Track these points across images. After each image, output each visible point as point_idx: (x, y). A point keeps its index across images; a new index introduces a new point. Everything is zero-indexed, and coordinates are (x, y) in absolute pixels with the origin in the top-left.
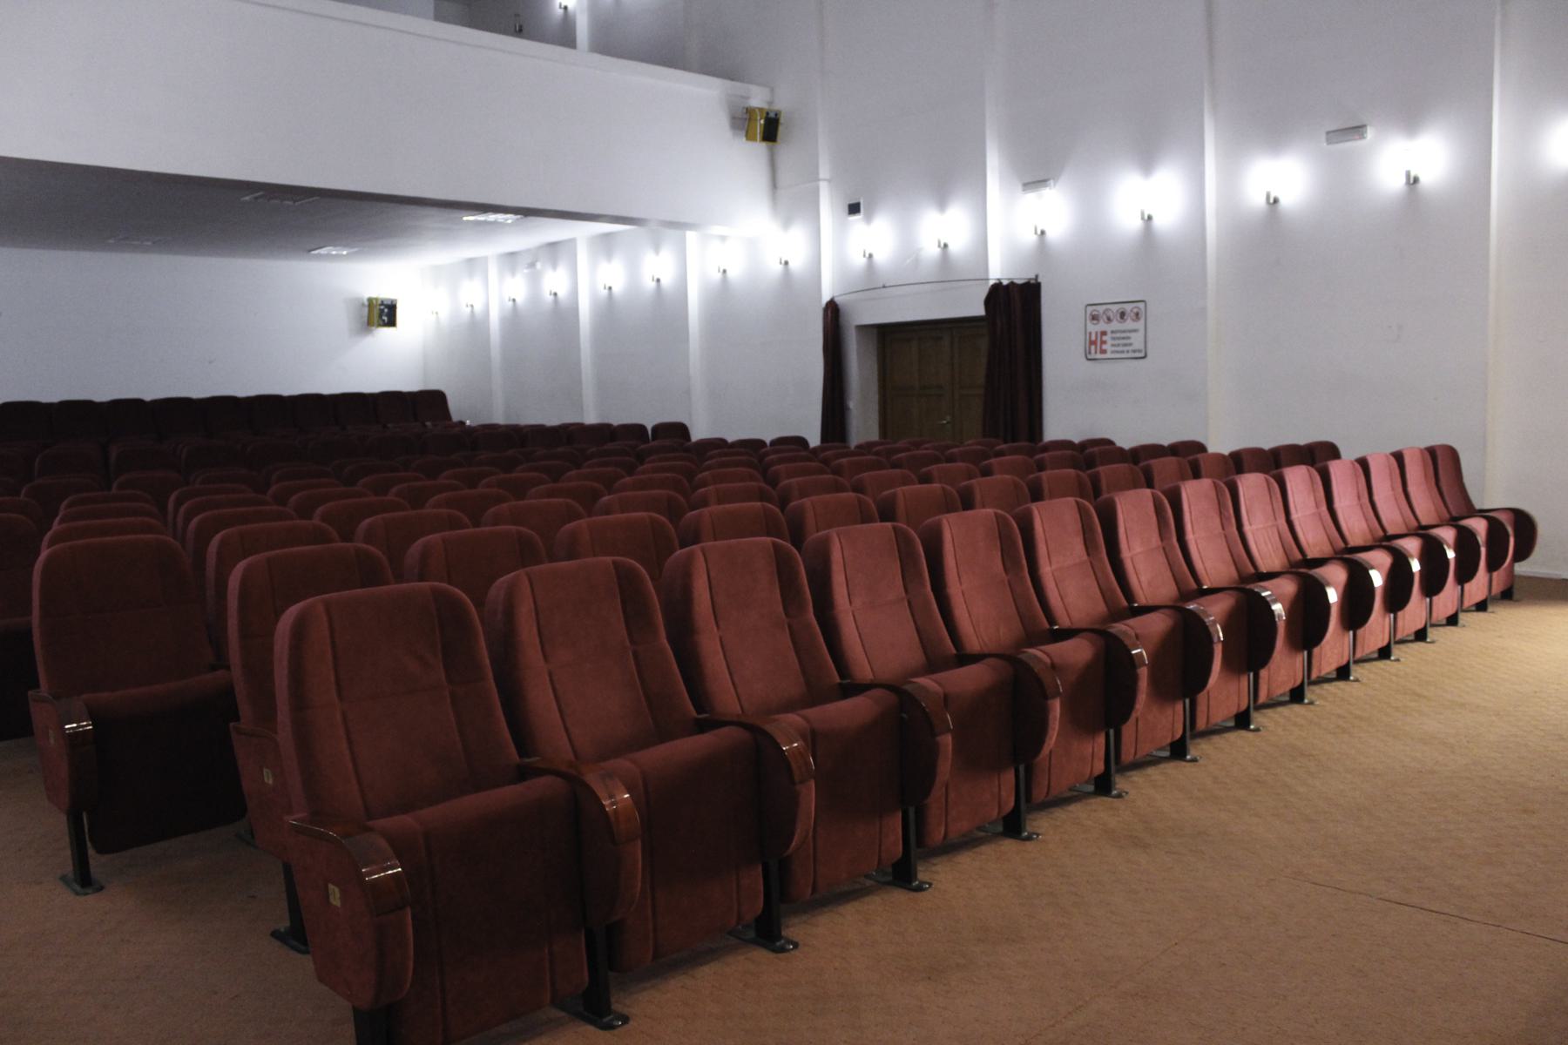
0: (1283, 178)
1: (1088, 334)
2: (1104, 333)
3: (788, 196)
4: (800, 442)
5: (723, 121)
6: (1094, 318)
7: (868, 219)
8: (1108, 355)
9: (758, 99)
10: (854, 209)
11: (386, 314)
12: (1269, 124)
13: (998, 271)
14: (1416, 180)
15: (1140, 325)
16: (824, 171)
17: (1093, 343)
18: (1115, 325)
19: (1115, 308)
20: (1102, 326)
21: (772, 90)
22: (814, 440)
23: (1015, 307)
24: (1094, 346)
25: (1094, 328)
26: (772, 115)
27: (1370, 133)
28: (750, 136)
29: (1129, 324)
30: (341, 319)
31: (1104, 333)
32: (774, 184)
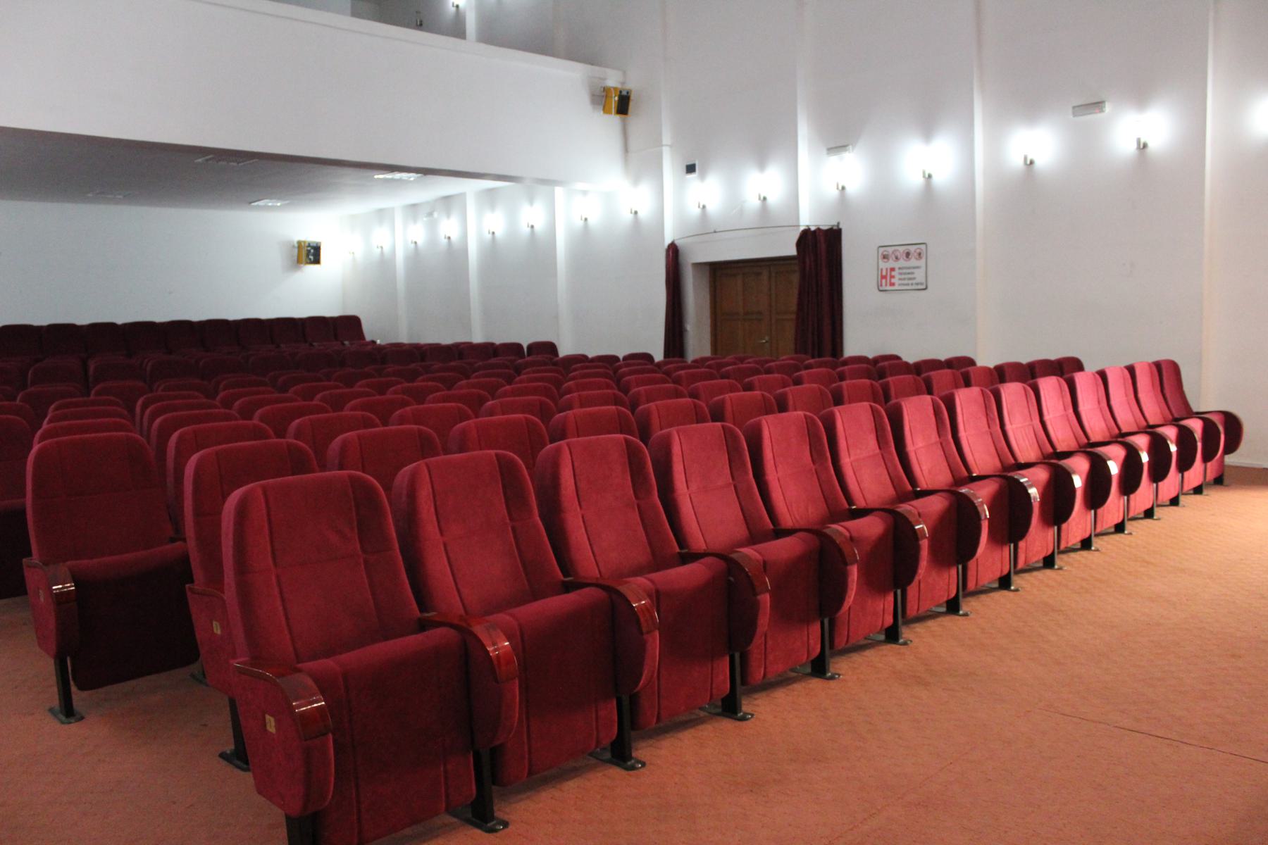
0: (1037, 144)
1: (879, 270)
2: (892, 269)
3: (637, 159)
4: (647, 357)
5: (585, 98)
6: (885, 257)
7: (702, 177)
8: (896, 287)
9: (613, 80)
10: (691, 169)
11: (312, 254)
12: (1026, 100)
13: (808, 219)
14: (1145, 146)
15: (922, 263)
16: (667, 138)
17: (883, 277)
18: (902, 263)
19: (901, 249)
20: (891, 264)
21: (624, 73)
22: (659, 356)
23: (821, 250)
24: (885, 280)
25: (885, 265)
26: (624, 93)
27: (1108, 108)
28: (606, 110)
29: (913, 262)
30: (276, 258)
31: (892, 269)
32: (626, 149)
